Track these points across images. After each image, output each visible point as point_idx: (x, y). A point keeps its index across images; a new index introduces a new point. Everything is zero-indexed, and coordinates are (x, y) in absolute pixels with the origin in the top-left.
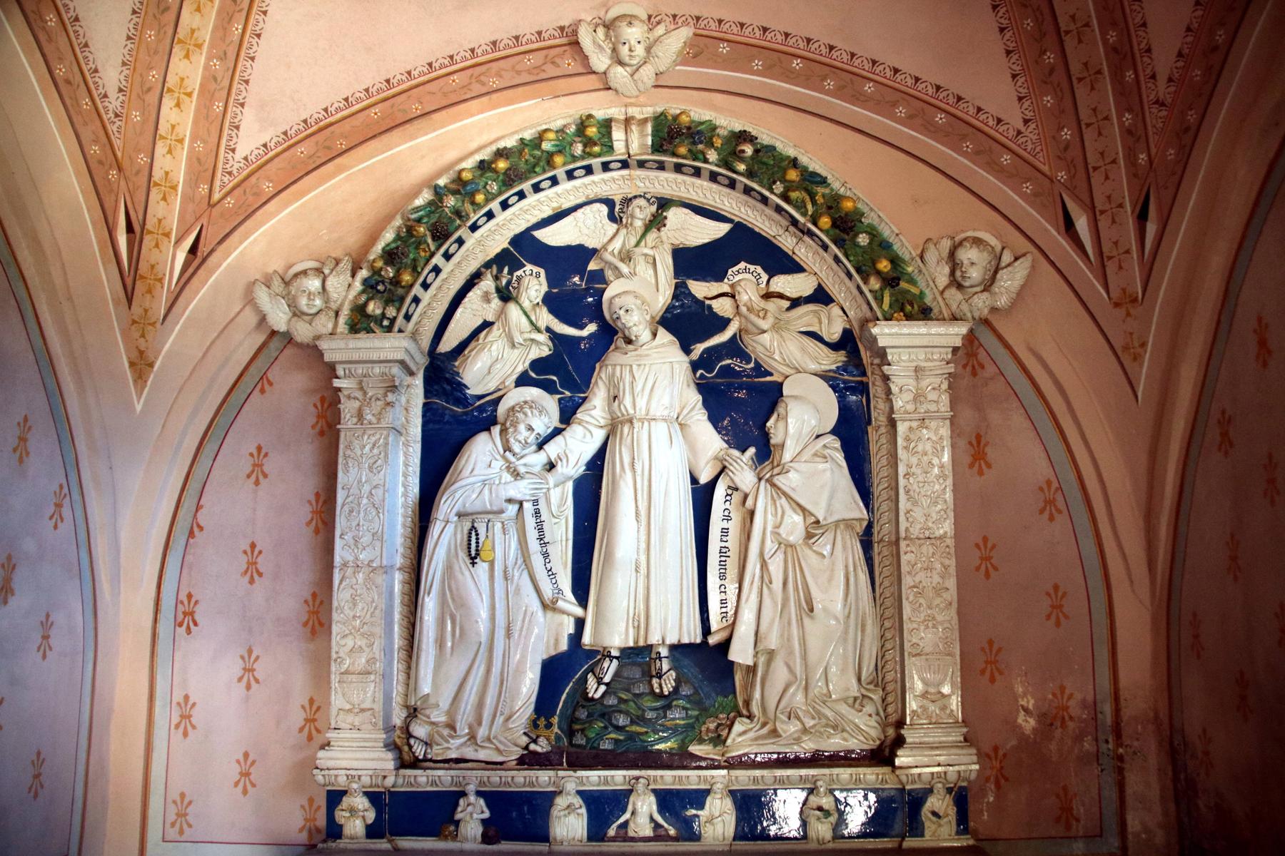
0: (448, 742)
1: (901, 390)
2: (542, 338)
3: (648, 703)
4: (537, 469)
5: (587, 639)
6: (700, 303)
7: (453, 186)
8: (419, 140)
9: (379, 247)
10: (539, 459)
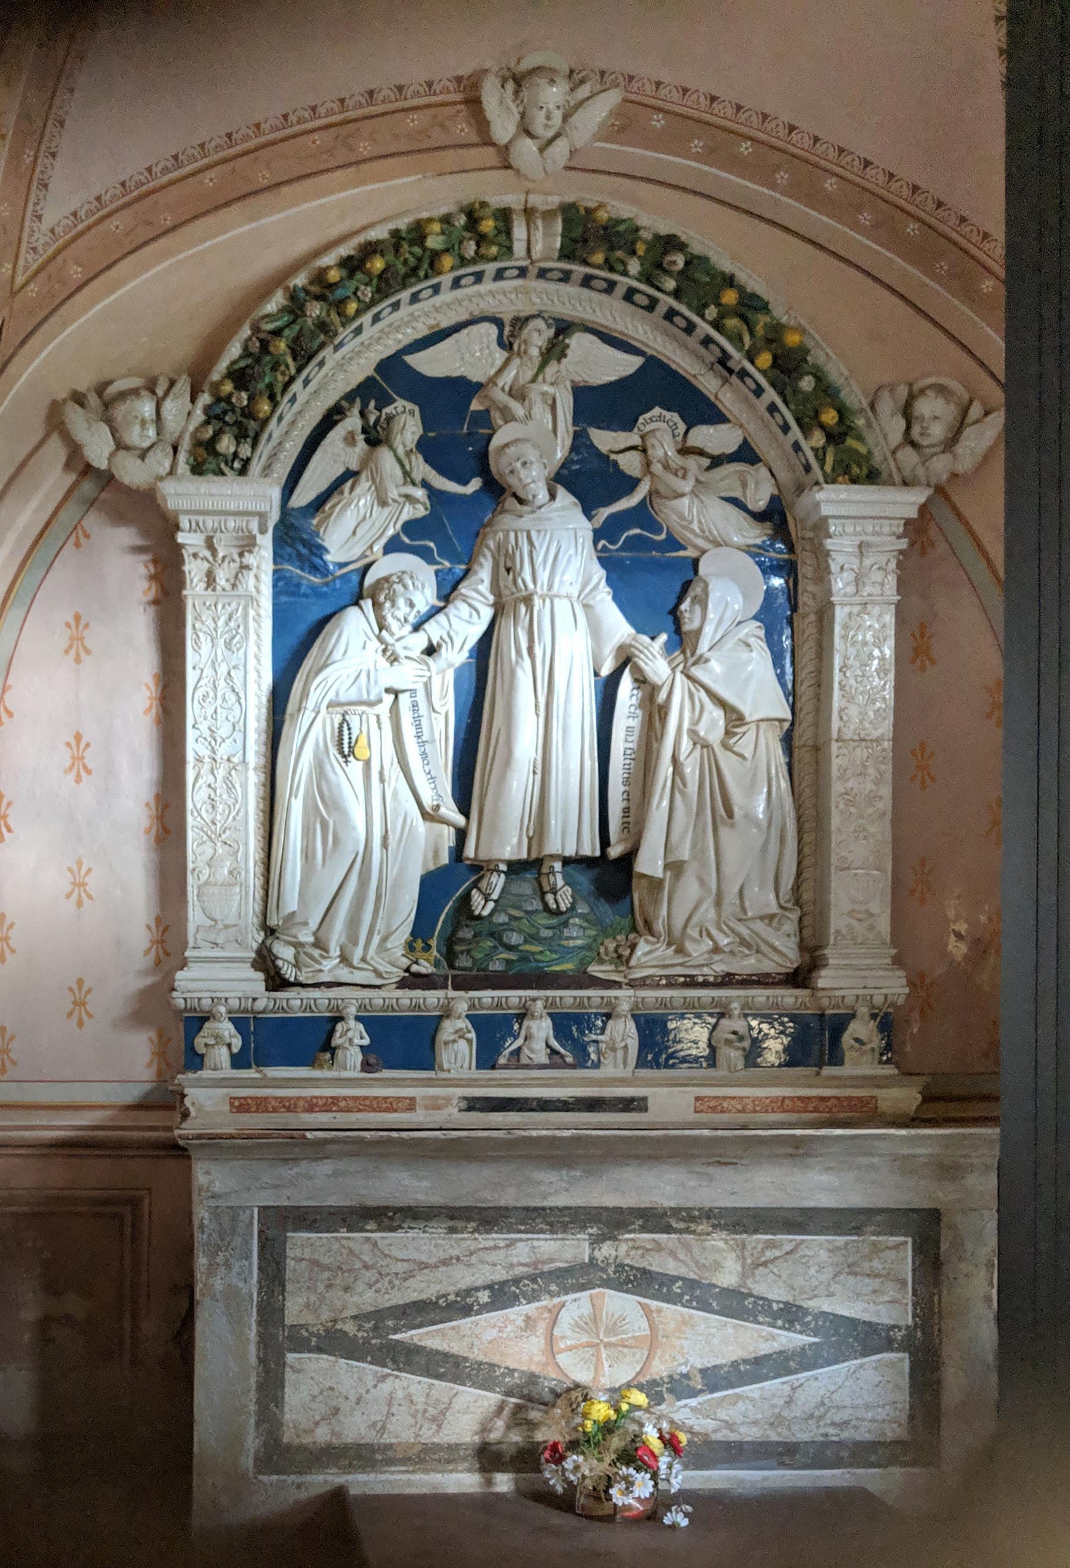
0: (320, 963)
1: (842, 568)
2: (420, 493)
3: (543, 920)
4: (416, 653)
5: (470, 851)
6: (604, 458)
7: (315, 289)
8: (264, 221)
9: (223, 365)
10: (420, 641)
